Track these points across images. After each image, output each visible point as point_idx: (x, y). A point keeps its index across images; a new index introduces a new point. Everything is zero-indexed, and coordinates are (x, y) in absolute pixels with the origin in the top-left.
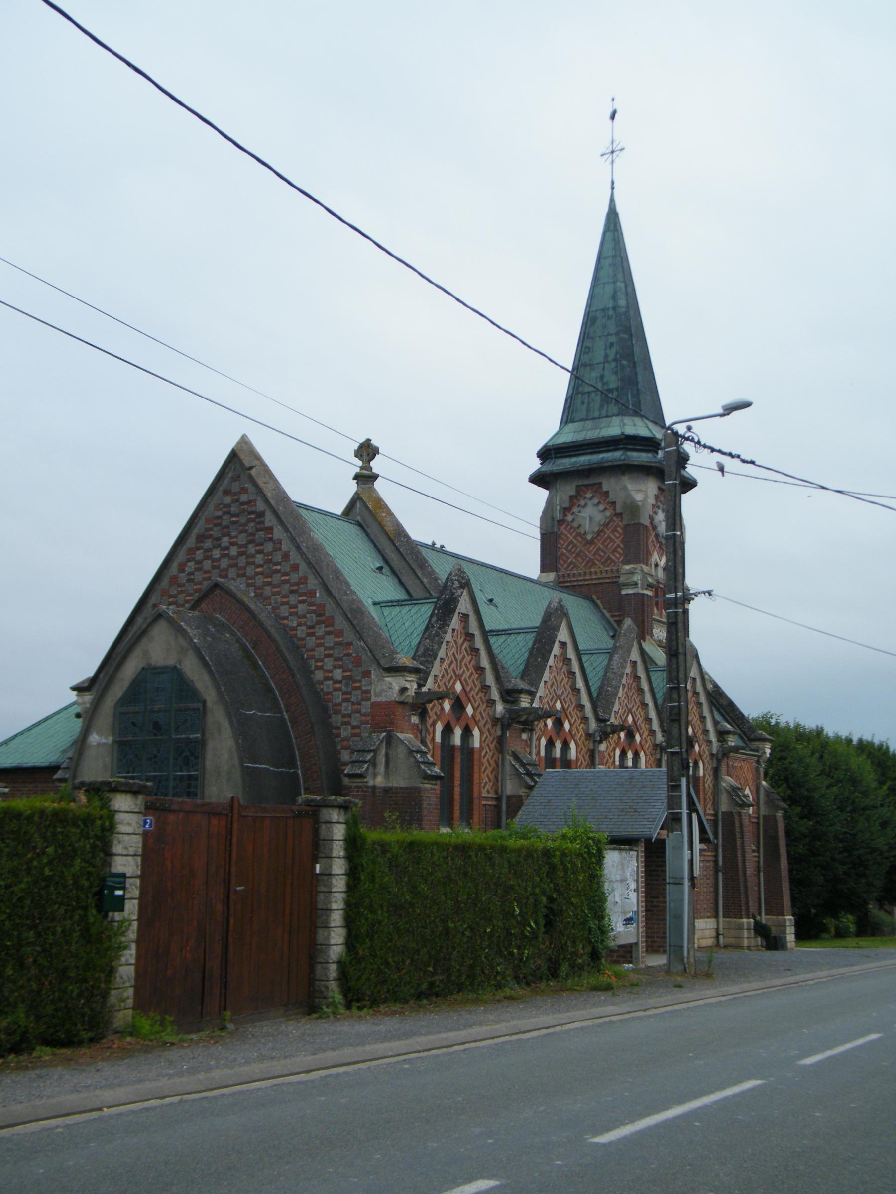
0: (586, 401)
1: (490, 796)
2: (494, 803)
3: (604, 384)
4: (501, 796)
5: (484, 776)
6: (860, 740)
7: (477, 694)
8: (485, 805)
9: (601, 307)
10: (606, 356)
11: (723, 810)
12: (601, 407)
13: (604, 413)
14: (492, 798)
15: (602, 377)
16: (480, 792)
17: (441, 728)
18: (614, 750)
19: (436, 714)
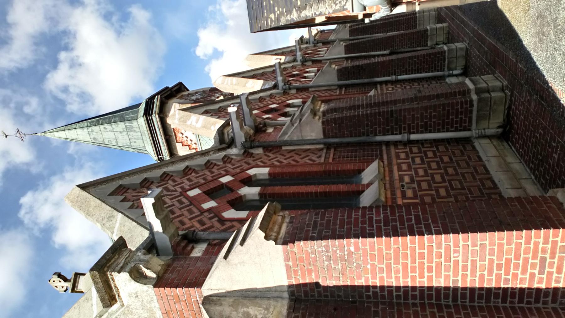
0: (134, 140)
1: (324, 155)
2: (332, 151)
3: (124, 131)
4: (325, 144)
5: (302, 162)
6: (359, 238)
7: (212, 173)
8: (334, 159)
9: (88, 136)
10: (110, 131)
11: (348, 37)
12: (135, 131)
13: (138, 130)
14: (326, 153)
15: (121, 132)
16: (320, 164)
17: (233, 211)
18: (301, 82)
19: (211, 219)
